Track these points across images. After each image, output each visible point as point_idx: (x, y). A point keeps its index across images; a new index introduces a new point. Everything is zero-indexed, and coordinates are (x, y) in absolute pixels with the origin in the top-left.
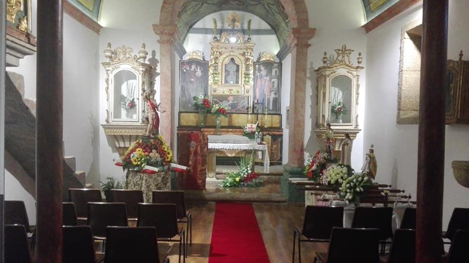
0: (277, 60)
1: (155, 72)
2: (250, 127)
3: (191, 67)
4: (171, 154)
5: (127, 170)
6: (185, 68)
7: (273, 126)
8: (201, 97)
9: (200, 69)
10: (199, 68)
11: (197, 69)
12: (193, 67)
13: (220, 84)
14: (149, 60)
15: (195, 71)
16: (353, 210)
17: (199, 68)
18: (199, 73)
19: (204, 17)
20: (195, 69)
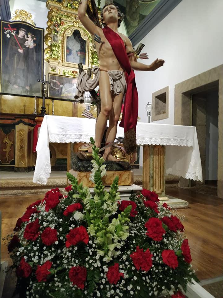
0: (36, 211)
1: (129, 277)
2: (155, 231)
3: (18, 33)
4: (9, 146)
5: (121, 270)
6: (9, 33)
7: (26, 113)
8: (85, 204)
9: (32, 38)
10: (30, 36)
11: (28, 37)
12: (22, 33)
13: (60, 60)
14: (125, 271)
15: (24, 40)
16: (47, 96)
17: (30, 36)
18: (30, 43)
19: (143, 38)
20: (24, 37)
